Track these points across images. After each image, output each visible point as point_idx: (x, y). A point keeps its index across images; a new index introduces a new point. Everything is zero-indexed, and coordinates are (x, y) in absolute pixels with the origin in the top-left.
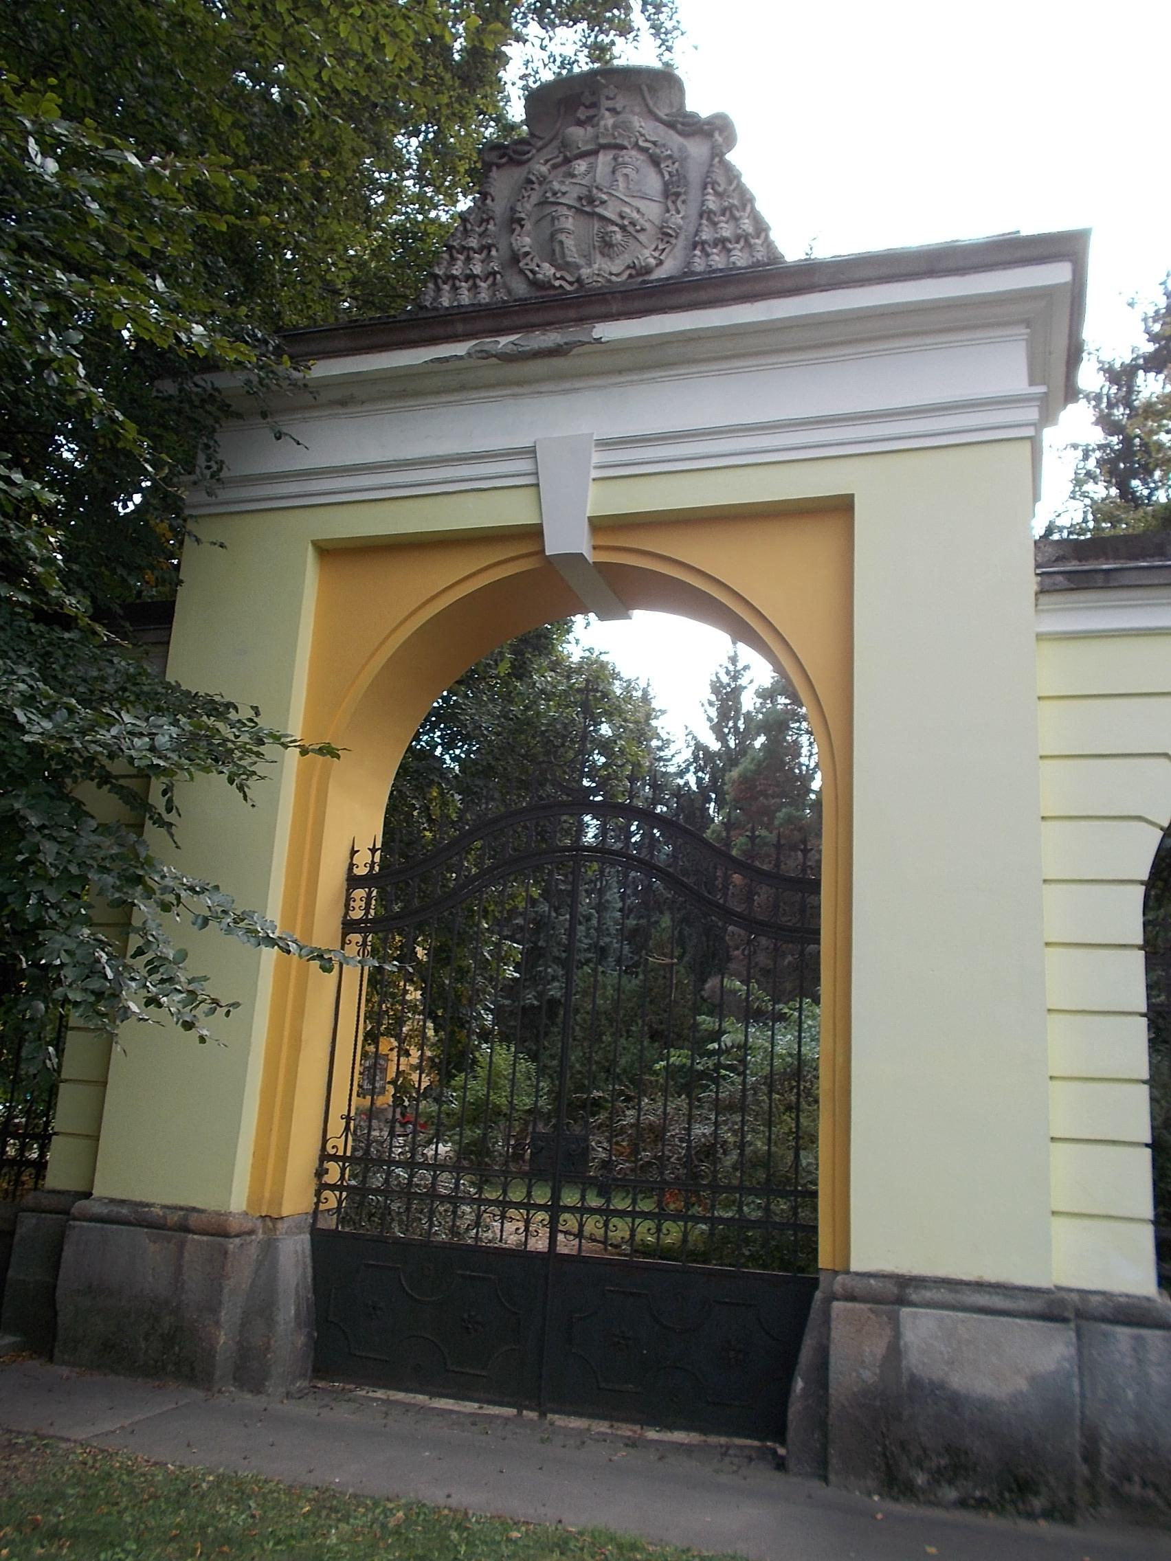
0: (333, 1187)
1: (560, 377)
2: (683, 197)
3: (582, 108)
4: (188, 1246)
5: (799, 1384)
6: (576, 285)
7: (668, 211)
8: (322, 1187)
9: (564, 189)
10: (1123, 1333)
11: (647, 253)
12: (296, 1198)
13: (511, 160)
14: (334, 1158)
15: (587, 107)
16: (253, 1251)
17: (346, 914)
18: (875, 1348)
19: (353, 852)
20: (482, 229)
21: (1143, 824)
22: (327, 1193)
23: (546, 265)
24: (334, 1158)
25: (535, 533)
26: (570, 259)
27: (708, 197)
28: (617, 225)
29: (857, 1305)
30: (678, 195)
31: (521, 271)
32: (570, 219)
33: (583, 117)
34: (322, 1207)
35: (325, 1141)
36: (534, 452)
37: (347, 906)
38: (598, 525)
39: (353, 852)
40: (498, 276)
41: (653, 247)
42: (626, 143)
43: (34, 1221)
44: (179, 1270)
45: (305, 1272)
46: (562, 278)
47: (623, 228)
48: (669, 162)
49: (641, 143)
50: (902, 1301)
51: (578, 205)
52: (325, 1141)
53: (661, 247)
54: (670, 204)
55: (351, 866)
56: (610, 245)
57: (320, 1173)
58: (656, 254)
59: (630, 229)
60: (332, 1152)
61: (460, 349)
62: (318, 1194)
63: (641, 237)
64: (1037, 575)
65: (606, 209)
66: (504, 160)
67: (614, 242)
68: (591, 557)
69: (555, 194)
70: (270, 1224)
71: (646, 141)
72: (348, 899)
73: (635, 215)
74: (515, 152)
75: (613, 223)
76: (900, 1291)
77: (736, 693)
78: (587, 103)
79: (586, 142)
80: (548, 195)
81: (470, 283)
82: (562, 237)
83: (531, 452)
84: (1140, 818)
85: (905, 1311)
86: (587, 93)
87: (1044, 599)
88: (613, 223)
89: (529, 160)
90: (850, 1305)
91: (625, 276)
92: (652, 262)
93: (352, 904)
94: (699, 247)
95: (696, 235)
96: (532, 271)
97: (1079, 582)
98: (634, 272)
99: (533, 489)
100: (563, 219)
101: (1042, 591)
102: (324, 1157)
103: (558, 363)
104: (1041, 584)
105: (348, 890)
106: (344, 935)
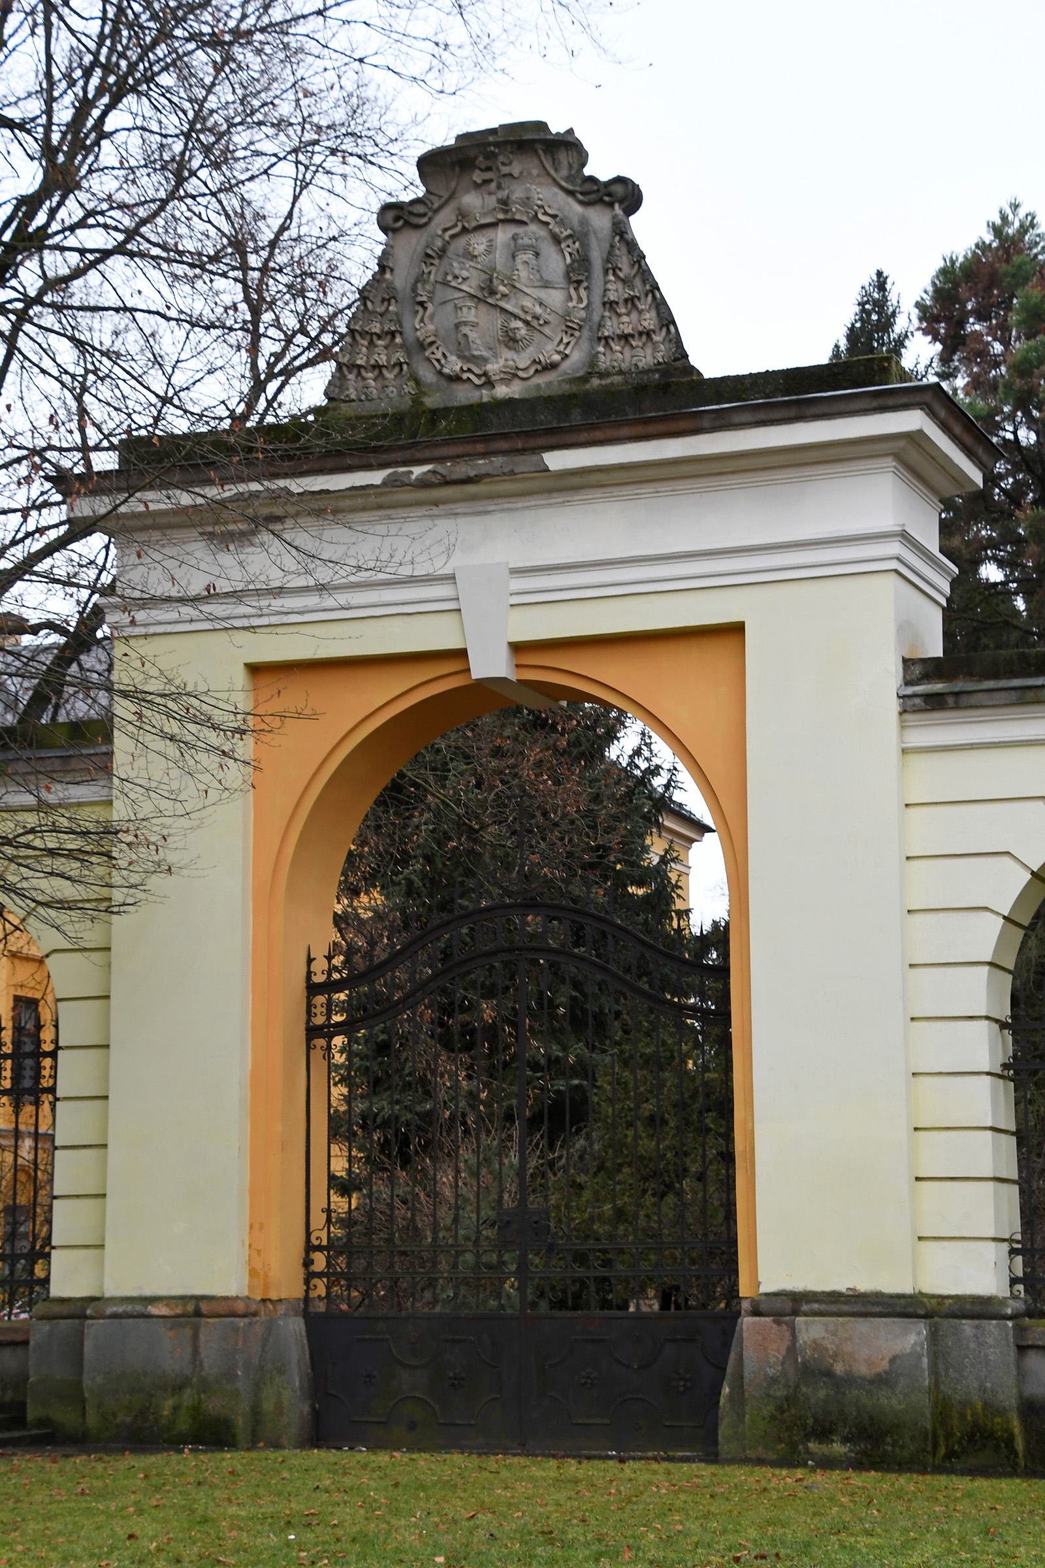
0: (319, 1275)
1: (474, 498)
2: (585, 284)
3: (477, 171)
4: (202, 1329)
5: (726, 1390)
6: (483, 379)
7: (571, 299)
8: (310, 1276)
9: (465, 274)
10: (967, 1326)
11: (550, 347)
12: (287, 1284)
13: (407, 223)
14: (319, 1248)
15: (482, 170)
16: (259, 1329)
17: (308, 1021)
18: (776, 1351)
19: (310, 960)
20: (383, 309)
21: (988, 914)
22: (316, 1281)
23: (453, 358)
24: (319, 1248)
25: (462, 654)
26: (476, 353)
27: (609, 286)
28: (520, 319)
29: (763, 1319)
30: (579, 282)
31: (428, 360)
32: (473, 311)
33: (479, 181)
34: (313, 1294)
35: (308, 1234)
36: (454, 578)
37: (309, 1012)
38: (517, 648)
39: (310, 960)
40: (405, 367)
41: (558, 339)
42: (525, 219)
43: (47, 1328)
44: (196, 1351)
45: (303, 1347)
46: (469, 370)
47: (527, 323)
48: (570, 242)
49: (541, 217)
50: (796, 1313)
51: (480, 296)
52: (308, 1234)
53: (565, 341)
54: (572, 291)
55: (309, 974)
56: (515, 341)
57: (307, 1263)
58: (561, 348)
59: (535, 323)
60: (316, 1243)
61: (376, 477)
62: (307, 1282)
63: (547, 330)
64: (904, 697)
65: (507, 302)
66: (400, 223)
67: (518, 337)
68: (513, 678)
69: (456, 277)
70: (271, 1307)
71: (545, 213)
72: (309, 1006)
73: (538, 310)
74: (411, 213)
75: (516, 317)
76: (794, 1304)
77: (1026, 232)
78: (483, 167)
79: (485, 214)
80: (449, 278)
81: (376, 372)
82: (465, 330)
83: (452, 578)
84: (986, 909)
85: (800, 1320)
86: (481, 159)
87: (907, 716)
88: (516, 317)
89: (426, 224)
90: (757, 1319)
91: (532, 371)
92: (557, 358)
93: (314, 1010)
94: (603, 342)
95: (604, 296)
96: (438, 361)
97: (934, 703)
98: (539, 367)
99: (455, 615)
100: (465, 310)
101: (903, 712)
102: (310, 1248)
103: (471, 489)
104: (903, 705)
105: (308, 998)
106: (309, 1040)
